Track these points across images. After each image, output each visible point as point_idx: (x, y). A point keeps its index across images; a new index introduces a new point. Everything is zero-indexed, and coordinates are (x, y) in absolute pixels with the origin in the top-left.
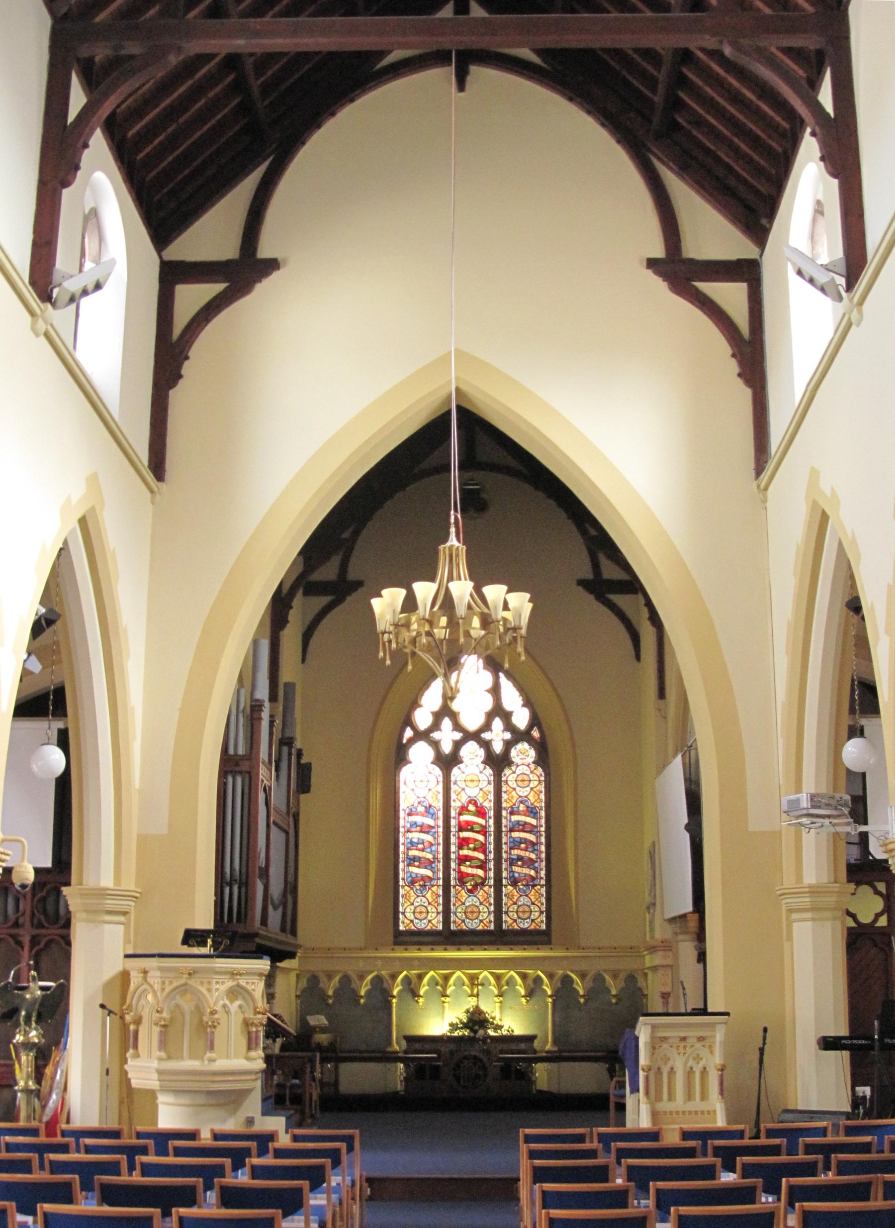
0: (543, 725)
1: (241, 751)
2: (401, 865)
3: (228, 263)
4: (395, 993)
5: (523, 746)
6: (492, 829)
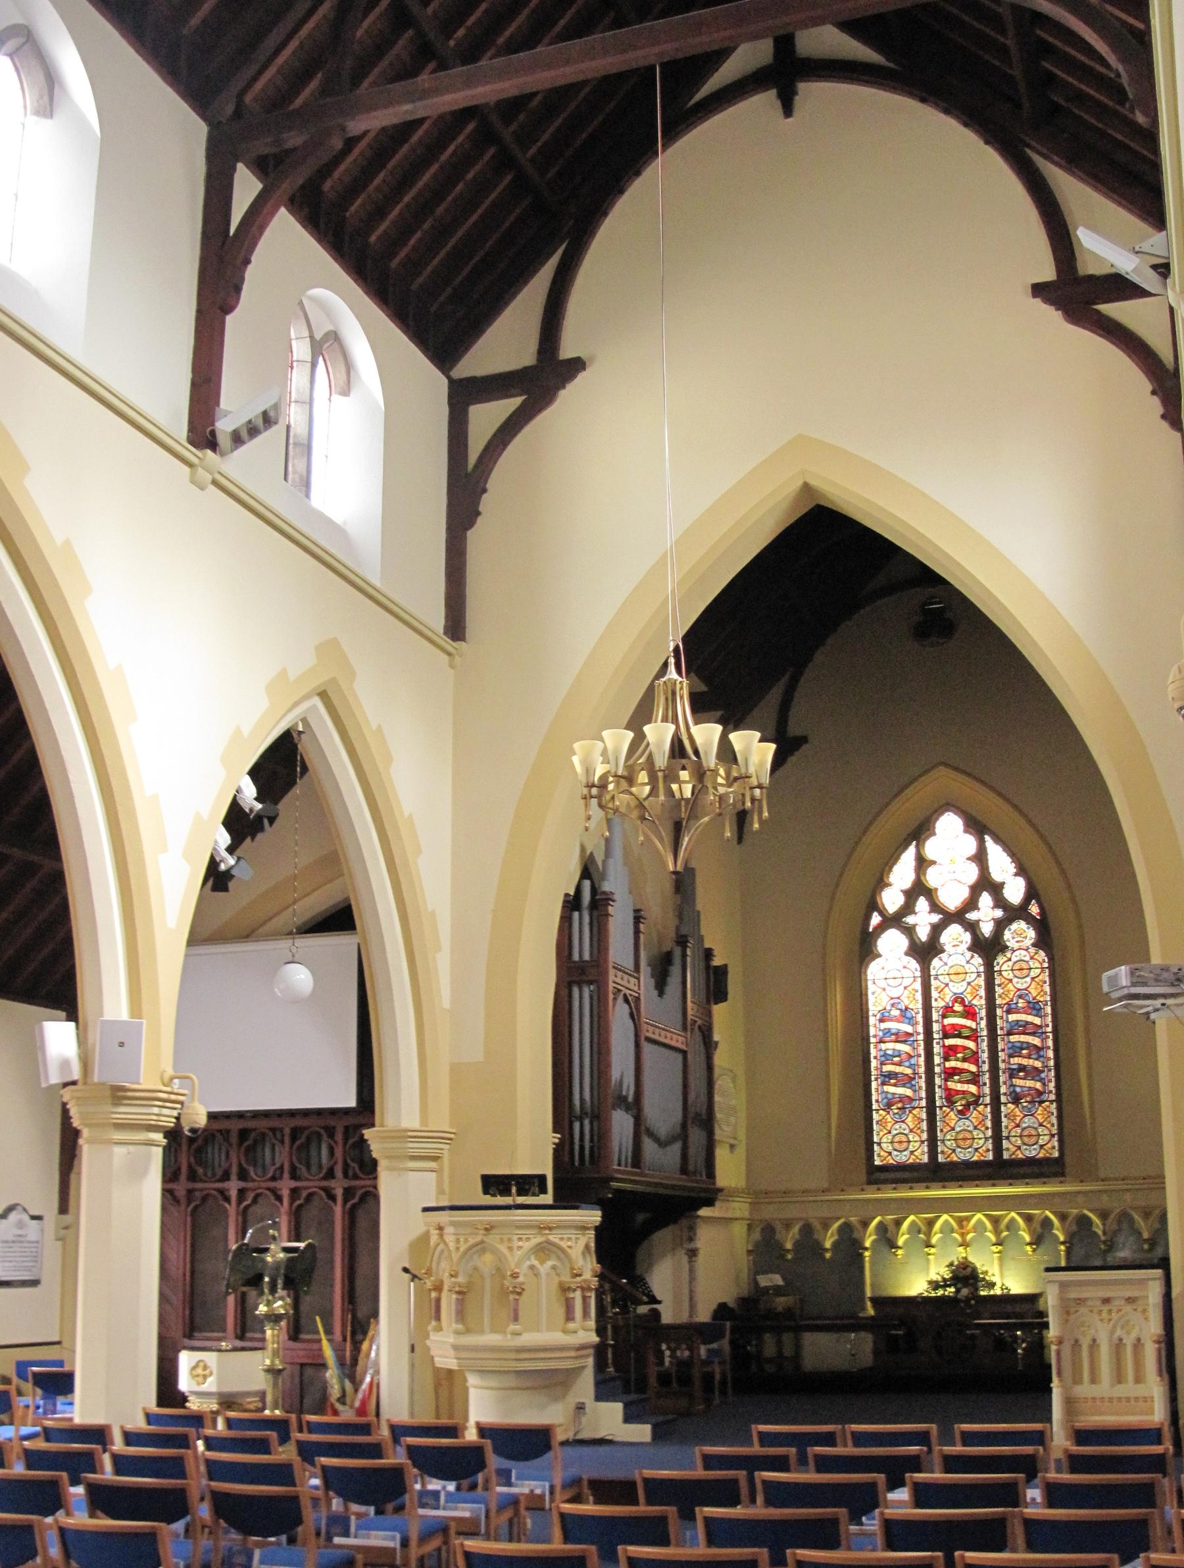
0: (1042, 898)
1: (587, 957)
2: (874, 1085)
3: (525, 370)
4: (867, 1244)
5: (1020, 925)
6: (985, 1033)
